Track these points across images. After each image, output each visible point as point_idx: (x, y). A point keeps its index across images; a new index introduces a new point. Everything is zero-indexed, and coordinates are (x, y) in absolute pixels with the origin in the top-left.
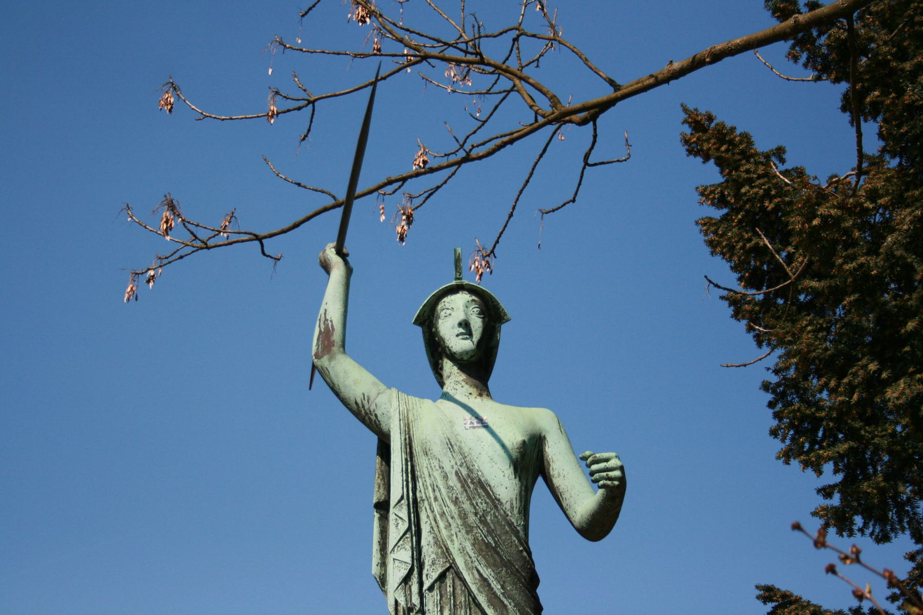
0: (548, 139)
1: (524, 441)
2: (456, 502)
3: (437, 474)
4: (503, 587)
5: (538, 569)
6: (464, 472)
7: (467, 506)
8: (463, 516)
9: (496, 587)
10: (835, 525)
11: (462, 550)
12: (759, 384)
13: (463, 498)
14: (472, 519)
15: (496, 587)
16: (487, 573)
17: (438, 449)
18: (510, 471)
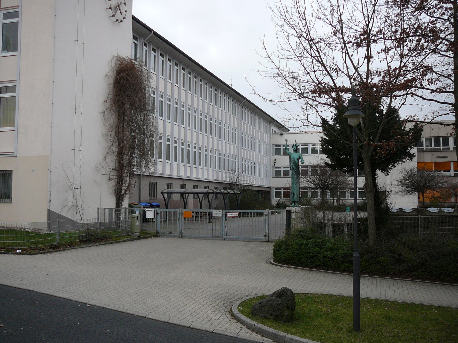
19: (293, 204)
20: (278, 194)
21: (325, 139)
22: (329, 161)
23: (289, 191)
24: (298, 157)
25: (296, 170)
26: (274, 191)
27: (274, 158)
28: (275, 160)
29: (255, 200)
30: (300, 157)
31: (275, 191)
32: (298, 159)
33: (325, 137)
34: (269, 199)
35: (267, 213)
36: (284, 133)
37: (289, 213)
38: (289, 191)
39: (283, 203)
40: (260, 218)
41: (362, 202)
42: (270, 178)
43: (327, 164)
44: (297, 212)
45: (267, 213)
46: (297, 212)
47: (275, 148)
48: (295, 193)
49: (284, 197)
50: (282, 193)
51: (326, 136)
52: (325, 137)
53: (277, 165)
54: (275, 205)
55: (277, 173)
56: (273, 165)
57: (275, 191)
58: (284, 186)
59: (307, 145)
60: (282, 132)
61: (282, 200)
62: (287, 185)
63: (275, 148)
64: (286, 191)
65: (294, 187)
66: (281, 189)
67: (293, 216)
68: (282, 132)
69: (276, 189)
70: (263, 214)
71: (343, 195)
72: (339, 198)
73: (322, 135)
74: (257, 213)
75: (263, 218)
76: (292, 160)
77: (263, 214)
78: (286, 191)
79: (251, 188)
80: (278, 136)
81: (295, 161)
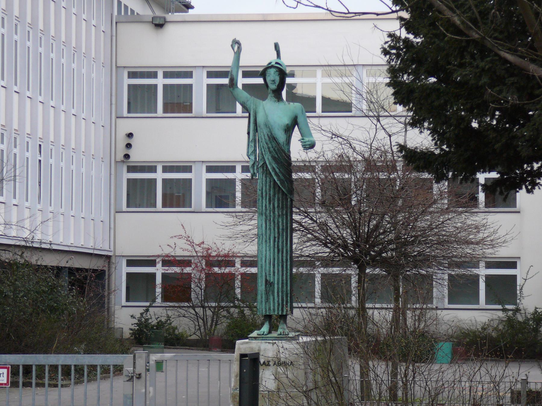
0: (144, 399)
1: (288, 124)
2: (267, 143)
3: (262, 134)
4: (279, 170)
5: (291, 150)
6: (269, 134)
7: (270, 145)
8: (269, 148)
9: (277, 170)
10: (440, 153)
11: (268, 159)
12: (276, 42)
13: (268, 142)
14: (272, 149)
15: (277, 170)
16: (275, 166)
17: (262, 126)
18: (283, 133)
19: (265, 328)
20: (140, 286)
21: (406, 40)
22: (421, 139)
23: (188, 270)
24: (286, 120)
25: (277, 182)
26: (123, 270)
27: (126, 126)
28: (130, 135)
29: (53, 310)
30: (295, 122)
31: (125, 270)
32: (289, 130)
33: (404, 34)
34: (101, 303)
35: (140, 369)
36: (170, 17)
37: (251, 364)
38: (188, 270)
39: (160, 325)
40: (66, 393)
41: (501, 321)
42: (104, 215)
43: (414, 158)
44: (284, 364)
45: (140, 369)
46: (284, 364)
47: (127, 81)
48: (275, 279)
49: (165, 298)
50: (159, 280)
51: (408, 31)
52: (404, 34)
53: (138, 156)
54: (127, 334)
55: (139, 195)
56: (120, 157)
57: (125, 270)
58: (167, 251)
59: (189, 75)
60: (159, 13)
61: (159, 311)
62: (182, 243)
63: (127, 81)
64: (177, 270)
65: (268, 253)
66: (152, 263)
67: (267, 379)
68: (159, 13)
69: (131, 263)
70: (119, 369)
71: (422, 288)
72: (405, 303)
73: (395, 27)
74: (54, 368)
75: (119, 384)
76: (263, 132)
77: (119, 369)
78: (177, 270)
79: (34, 259)
80: (145, 32)
81: (273, 138)
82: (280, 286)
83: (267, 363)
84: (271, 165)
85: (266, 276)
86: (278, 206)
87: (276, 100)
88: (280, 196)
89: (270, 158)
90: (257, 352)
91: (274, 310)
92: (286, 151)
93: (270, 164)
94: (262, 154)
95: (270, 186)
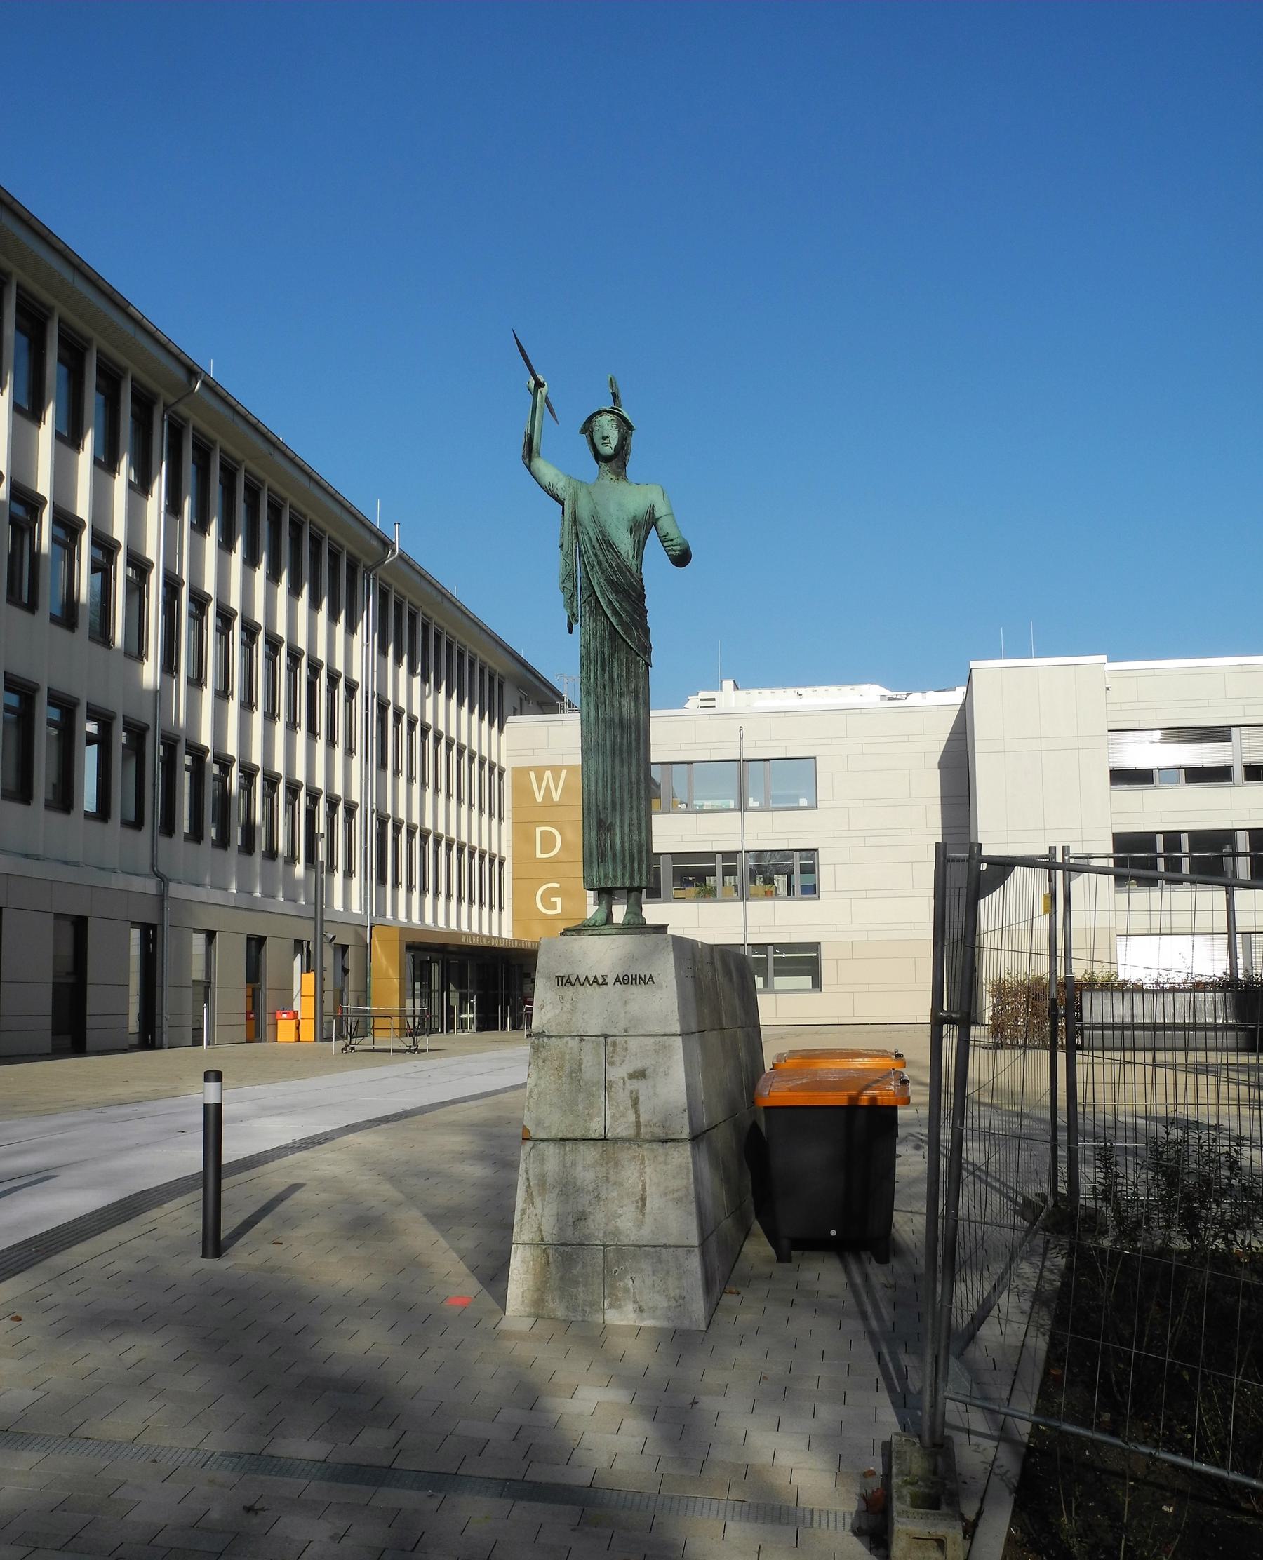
3: (586, 537)
8: (600, 563)
15: (616, 605)
16: (612, 597)
82: (627, 830)
83: (600, 981)
84: (605, 597)
85: (598, 812)
86: (620, 676)
87: (614, 477)
88: (623, 655)
89: (602, 581)
90: (892, 1104)
91: (615, 877)
92: (634, 569)
93: (603, 594)
94: (588, 577)
95: (603, 638)
